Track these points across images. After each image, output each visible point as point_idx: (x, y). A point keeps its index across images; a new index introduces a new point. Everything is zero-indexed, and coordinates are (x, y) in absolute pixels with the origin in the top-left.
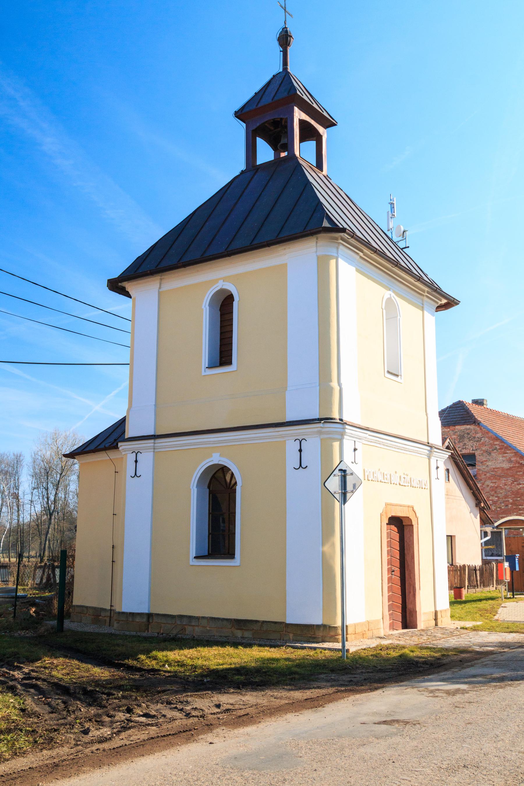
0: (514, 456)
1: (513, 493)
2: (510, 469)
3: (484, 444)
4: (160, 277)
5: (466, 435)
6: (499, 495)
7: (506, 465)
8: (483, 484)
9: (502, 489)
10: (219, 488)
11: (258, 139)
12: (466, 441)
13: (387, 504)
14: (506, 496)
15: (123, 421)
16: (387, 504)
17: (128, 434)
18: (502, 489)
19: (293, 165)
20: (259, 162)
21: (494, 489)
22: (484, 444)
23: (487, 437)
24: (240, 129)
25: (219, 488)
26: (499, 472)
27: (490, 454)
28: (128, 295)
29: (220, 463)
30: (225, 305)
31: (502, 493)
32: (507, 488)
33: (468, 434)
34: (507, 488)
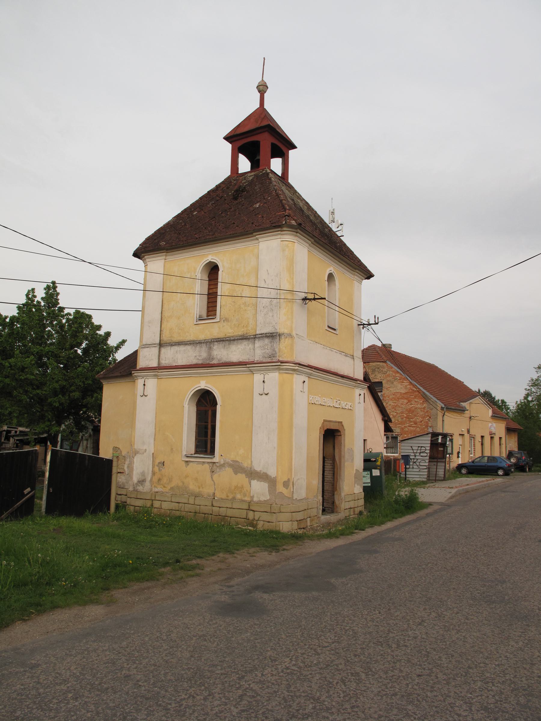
0: (409, 385)
1: (407, 410)
2: (406, 393)
3: (389, 376)
4: (164, 257)
5: (377, 369)
6: (398, 411)
7: (403, 391)
8: (387, 404)
9: (400, 407)
10: (206, 402)
11: (240, 154)
12: (377, 373)
13: (324, 421)
14: (402, 413)
15: (136, 353)
16: (324, 421)
17: (138, 368)
18: (400, 407)
19: (268, 175)
20: (280, 175)
21: (394, 407)
22: (389, 376)
23: (392, 371)
24: (228, 147)
25: (206, 402)
26: (398, 395)
27: (392, 383)
28: (153, 246)
29: (206, 388)
30: (213, 270)
31: (399, 410)
32: (403, 406)
33: (378, 368)
34: (403, 406)
